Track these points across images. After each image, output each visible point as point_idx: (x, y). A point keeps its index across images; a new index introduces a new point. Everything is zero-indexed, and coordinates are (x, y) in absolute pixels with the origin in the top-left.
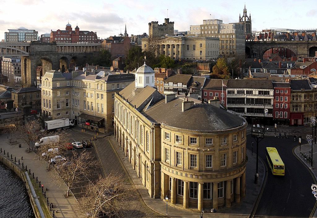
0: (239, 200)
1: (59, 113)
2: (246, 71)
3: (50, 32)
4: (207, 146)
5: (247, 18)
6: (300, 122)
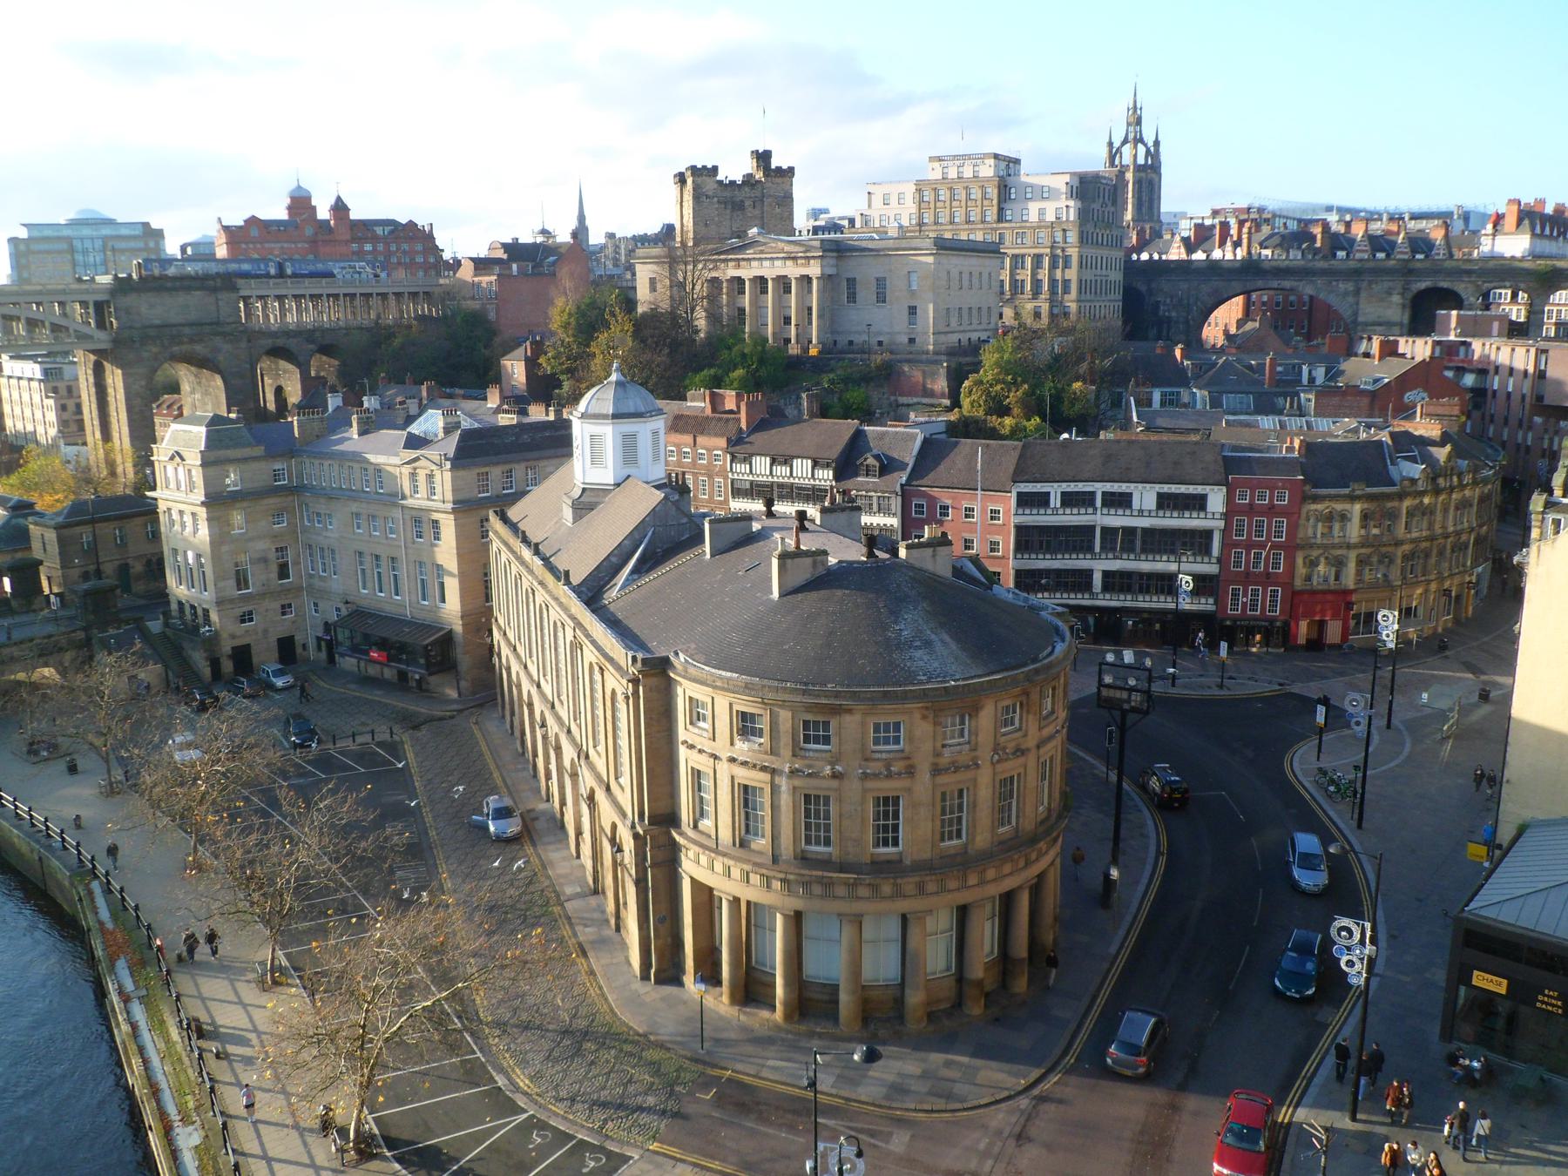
0: (1021, 985)
1: (250, 613)
2: (1118, 402)
3: (213, 232)
4: (878, 756)
5: (1141, 149)
6: (1333, 632)
